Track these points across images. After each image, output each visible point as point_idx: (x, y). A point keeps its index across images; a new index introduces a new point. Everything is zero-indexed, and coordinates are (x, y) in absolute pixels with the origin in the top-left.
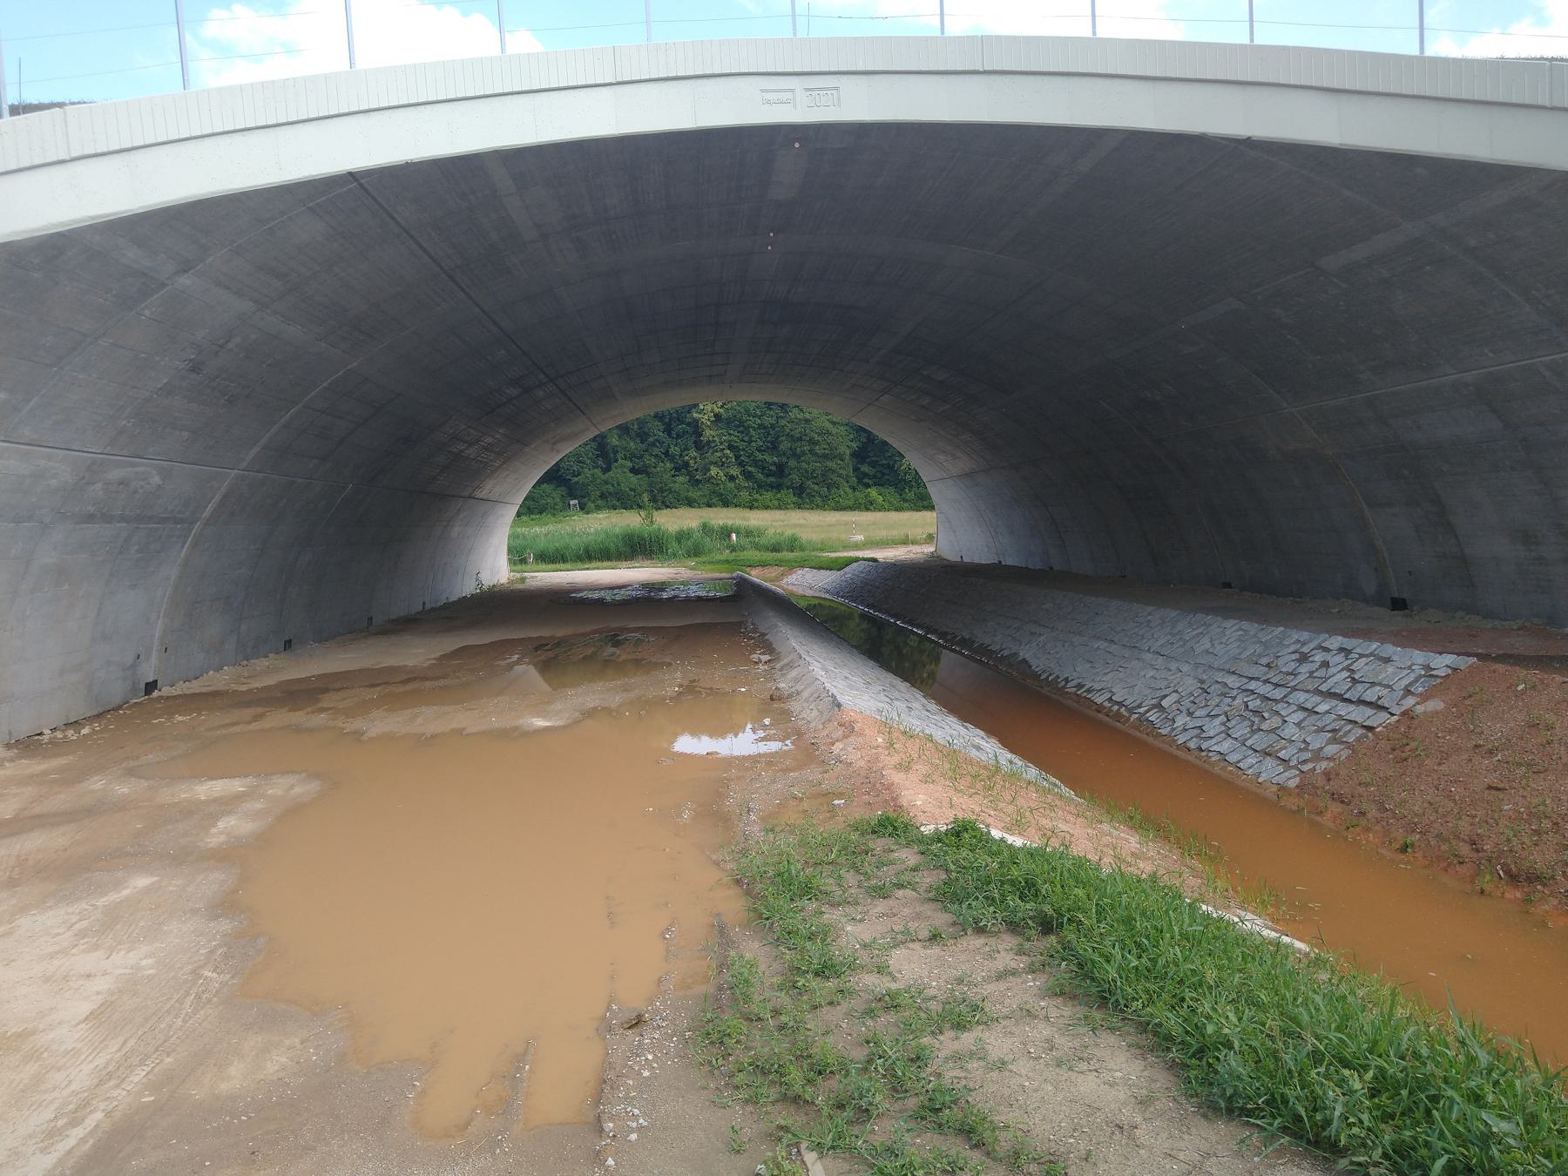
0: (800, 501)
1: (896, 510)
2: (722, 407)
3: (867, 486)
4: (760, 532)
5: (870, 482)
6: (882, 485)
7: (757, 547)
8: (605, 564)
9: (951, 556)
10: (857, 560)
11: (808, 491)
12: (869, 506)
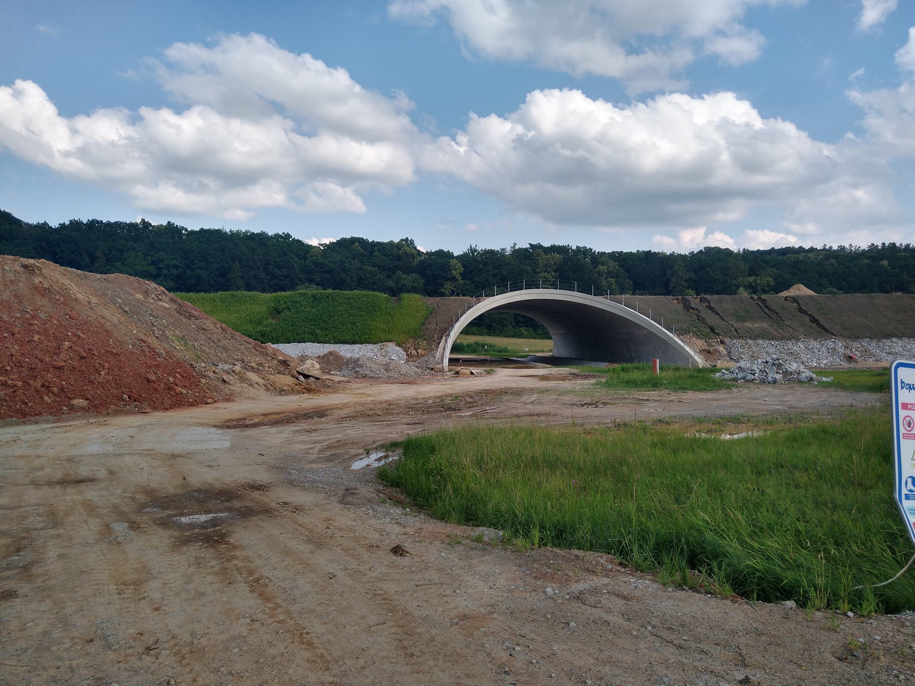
0: (489, 332)
1: (533, 338)
2: (455, 287)
3: (520, 327)
4: (495, 346)
5: (522, 325)
6: (527, 326)
7: (494, 351)
8: (654, 331)
9: (557, 355)
10: (530, 355)
11: (493, 327)
12: (521, 336)
